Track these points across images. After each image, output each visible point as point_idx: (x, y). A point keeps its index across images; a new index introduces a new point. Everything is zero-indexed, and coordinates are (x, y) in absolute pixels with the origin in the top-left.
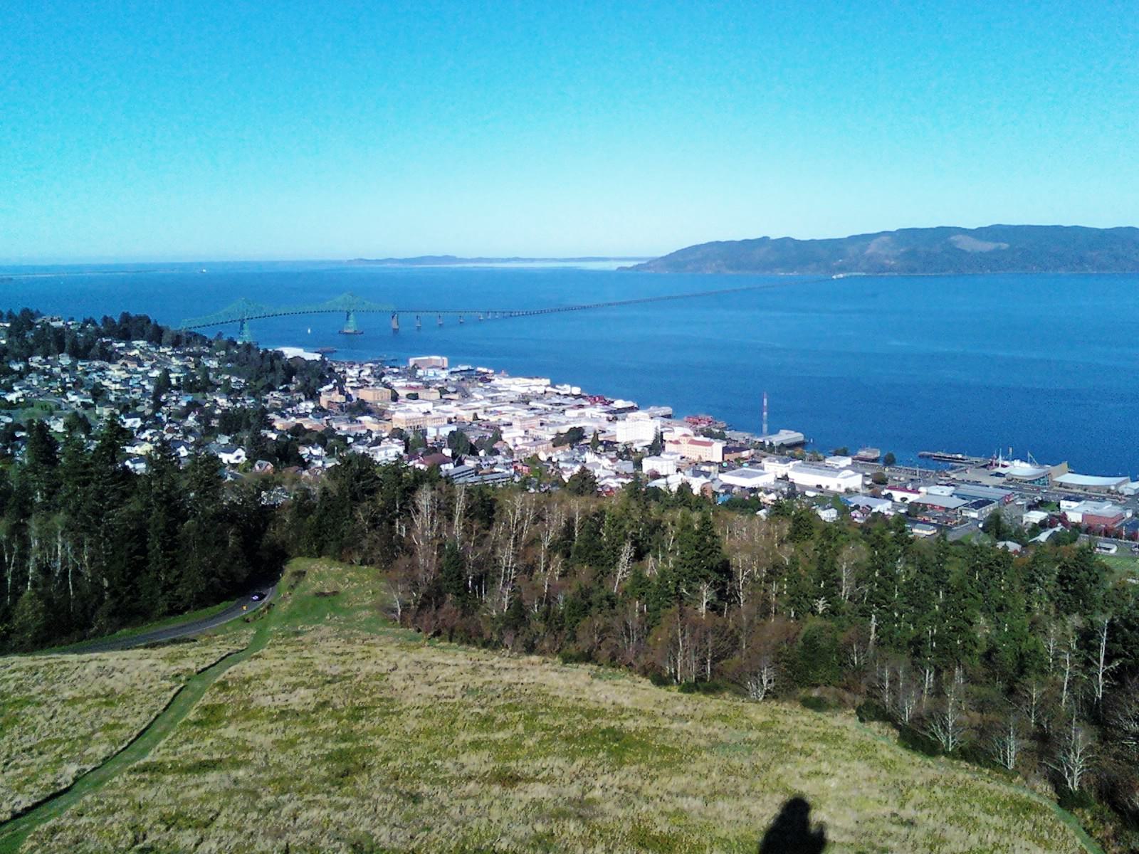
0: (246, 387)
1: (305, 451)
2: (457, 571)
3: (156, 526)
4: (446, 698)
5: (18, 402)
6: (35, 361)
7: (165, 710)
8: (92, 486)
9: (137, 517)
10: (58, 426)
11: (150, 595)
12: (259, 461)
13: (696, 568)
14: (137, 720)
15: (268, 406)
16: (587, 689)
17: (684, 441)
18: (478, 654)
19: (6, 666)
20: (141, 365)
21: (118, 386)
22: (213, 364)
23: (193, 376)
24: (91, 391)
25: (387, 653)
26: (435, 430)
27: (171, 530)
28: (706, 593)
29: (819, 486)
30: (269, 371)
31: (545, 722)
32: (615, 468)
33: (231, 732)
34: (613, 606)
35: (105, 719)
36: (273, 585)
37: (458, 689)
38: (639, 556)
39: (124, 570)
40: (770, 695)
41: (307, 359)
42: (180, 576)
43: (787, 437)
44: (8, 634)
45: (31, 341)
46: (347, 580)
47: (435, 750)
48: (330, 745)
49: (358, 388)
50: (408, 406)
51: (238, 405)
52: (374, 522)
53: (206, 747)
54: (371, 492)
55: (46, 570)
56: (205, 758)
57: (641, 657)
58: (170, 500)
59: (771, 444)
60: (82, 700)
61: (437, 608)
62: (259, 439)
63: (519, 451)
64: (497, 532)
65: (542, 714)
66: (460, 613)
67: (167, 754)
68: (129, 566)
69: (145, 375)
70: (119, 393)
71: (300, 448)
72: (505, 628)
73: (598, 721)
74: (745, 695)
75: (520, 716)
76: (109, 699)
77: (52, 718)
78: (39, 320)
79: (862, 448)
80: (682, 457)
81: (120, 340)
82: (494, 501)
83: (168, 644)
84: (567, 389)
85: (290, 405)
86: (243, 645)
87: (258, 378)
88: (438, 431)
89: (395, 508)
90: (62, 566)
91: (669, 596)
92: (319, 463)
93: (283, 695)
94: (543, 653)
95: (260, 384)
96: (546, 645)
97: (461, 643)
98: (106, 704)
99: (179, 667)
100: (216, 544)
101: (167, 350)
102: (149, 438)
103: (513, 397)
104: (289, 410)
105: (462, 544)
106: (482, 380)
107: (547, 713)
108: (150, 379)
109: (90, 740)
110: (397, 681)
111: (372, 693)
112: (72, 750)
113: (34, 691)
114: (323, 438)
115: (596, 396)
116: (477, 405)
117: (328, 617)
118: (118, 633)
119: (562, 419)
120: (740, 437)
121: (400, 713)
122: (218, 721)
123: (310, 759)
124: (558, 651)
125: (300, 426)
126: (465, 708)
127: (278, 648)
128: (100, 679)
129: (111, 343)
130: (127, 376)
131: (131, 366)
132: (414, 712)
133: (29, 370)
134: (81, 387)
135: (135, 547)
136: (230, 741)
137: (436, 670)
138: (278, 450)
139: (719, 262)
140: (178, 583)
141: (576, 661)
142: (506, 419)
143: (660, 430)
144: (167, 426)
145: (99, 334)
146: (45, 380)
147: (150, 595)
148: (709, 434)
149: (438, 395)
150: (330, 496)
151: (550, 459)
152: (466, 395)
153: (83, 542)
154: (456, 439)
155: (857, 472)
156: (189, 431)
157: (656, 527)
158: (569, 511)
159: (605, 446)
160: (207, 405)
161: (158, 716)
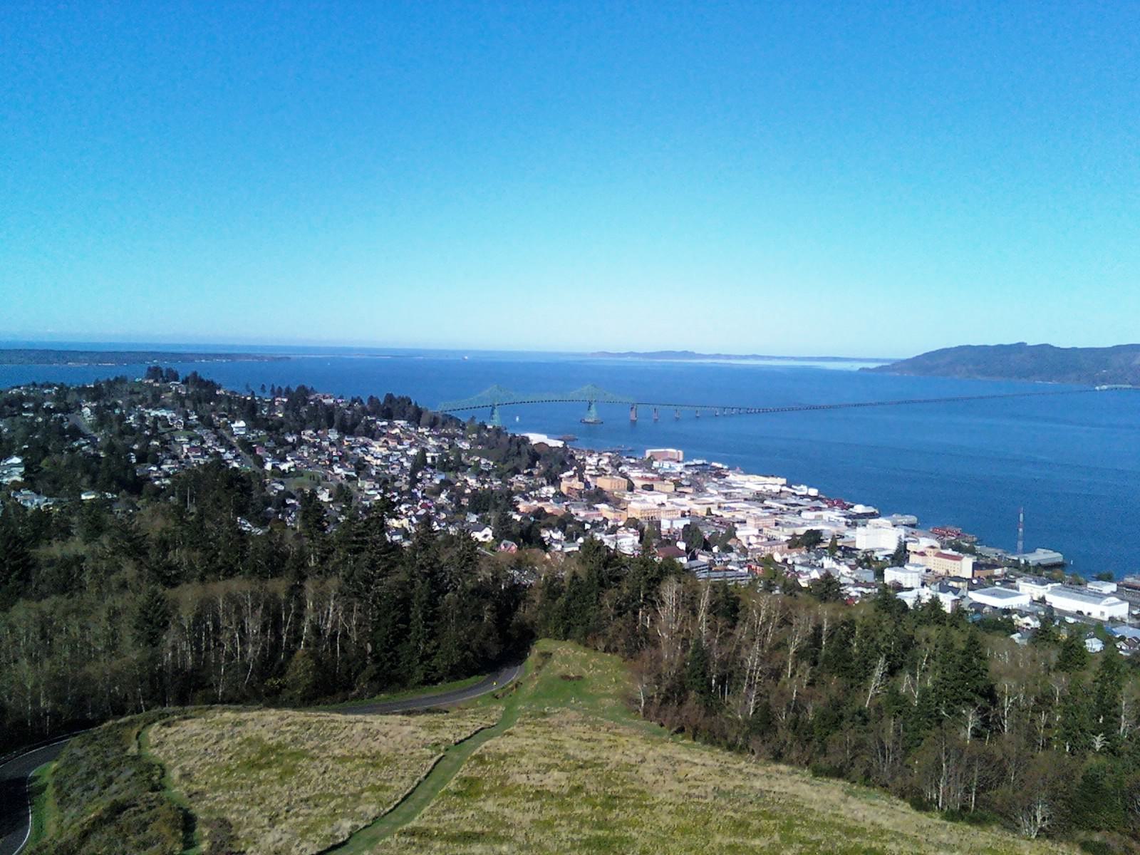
0: (494, 469)
1: (546, 534)
2: (701, 669)
3: (420, 597)
4: (698, 797)
5: (290, 472)
6: (307, 434)
7: (426, 777)
8: (366, 555)
9: (402, 586)
10: (324, 497)
11: (409, 663)
12: (505, 541)
13: (960, 690)
14: (401, 784)
15: (513, 489)
16: (842, 806)
17: (930, 552)
18: (725, 756)
19: (282, 719)
20: (400, 443)
21: (379, 462)
22: (465, 445)
23: (447, 456)
24: (355, 465)
25: (634, 745)
26: (669, 522)
27: (432, 602)
28: (972, 719)
29: (1080, 613)
30: (517, 455)
31: (802, 834)
32: (854, 576)
33: (490, 806)
34: (865, 721)
35: (372, 780)
36: (520, 664)
37: (709, 790)
38: (892, 671)
39: (387, 637)
40: (1044, 834)
41: (550, 445)
42: (438, 647)
43: (1044, 557)
44: (280, 689)
45: (304, 416)
46: (591, 666)
47: (692, 849)
48: (586, 831)
49: (596, 476)
50: (644, 496)
51: (486, 486)
52: (620, 611)
53: (466, 818)
54: (617, 579)
55: (317, 631)
56: (468, 829)
57: (898, 778)
58: (432, 573)
59: (1027, 563)
60: (351, 759)
61: (680, 703)
62: (506, 520)
63: (753, 550)
64: (741, 632)
65: (798, 825)
66: (703, 712)
67: (432, 821)
68: (393, 633)
69: (404, 453)
70: (380, 468)
71: (542, 531)
72: (750, 732)
73: (857, 840)
74: (1015, 831)
75: (775, 825)
76: (375, 761)
77: (325, 772)
78: (312, 397)
79: (1131, 574)
80: (927, 570)
81: (383, 418)
82: (738, 600)
83: (423, 713)
84: (803, 489)
85: (532, 489)
86: (493, 721)
87: (505, 462)
88: (672, 524)
89: (639, 598)
90: (332, 629)
91: (929, 717)
92: (559, 547)
93: (538, 775)
94: (790, 763)
95: (507, 467)
96: (794, 755)
97: (705, 743)
98: (373, 765)
99: (439, 736)
100: (473, 618)
101: (425, 430)
102: (404, 512)
103: (747, 494)
104: (532, 493)
105: (708, 641)
106: (716, 476)
107: (802, 825)
108: (408, 457)
109: (359, 798)
110: (647, 772)
111: (623, 784)
112: (343, 806)
113: (309, 745)
114: (563, 523)
115: (833, 497)
116: (711, 500)
117: (573, 701)
118: (376, 698)
119: (798, 520)
120: (991, 553)
121: (652, 807)
122: (478, 794)
123: (569, 843)
124: (807, 763)
125: (542, 509)
126: (718, 810)
127: (529, 728)
128: (366, 741)
129: (374, 422)
130: (388, 452)
131: (392, 444)
132: (667, 808)
133: (301, 442)
134: (346, 461)
135: (399, 615)
136: (490, 815)
137: (684, 768)
138: (522, 531)
139: (971, 367)
140: (435, 654)
141: (827, 775)
142: (739, 516)
143: (903, 539)
144: (422, 501)
145: (365, 412)
146: (314, 452)
147: (409, 663)
148: (958, 548)
149: (672, 487)
150: (579, 580)
151: (785, 561)
152: (700, 490)
153: (353, 607)
154: (690, 532)
155: (1123, 600)
156: (441, 508)
157: (908, 644)
158: (817, 617)
159: (844, 551)
160: (458, 484)
161: (420, 782)
